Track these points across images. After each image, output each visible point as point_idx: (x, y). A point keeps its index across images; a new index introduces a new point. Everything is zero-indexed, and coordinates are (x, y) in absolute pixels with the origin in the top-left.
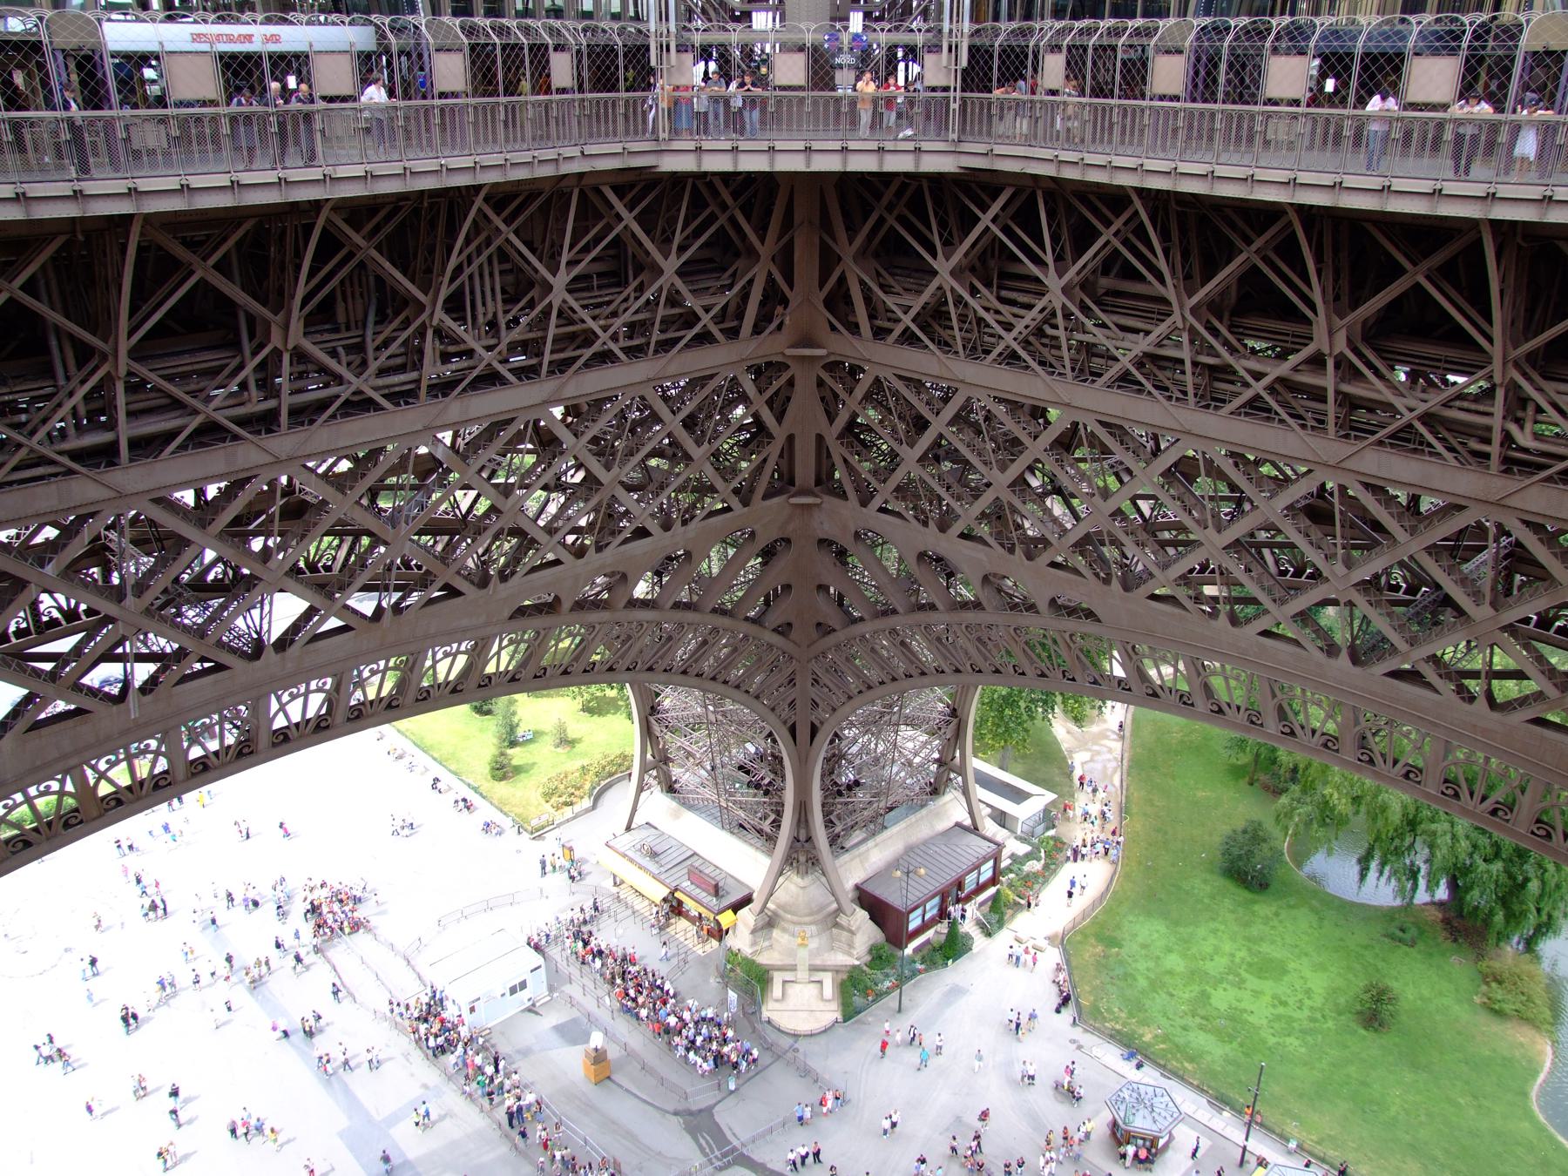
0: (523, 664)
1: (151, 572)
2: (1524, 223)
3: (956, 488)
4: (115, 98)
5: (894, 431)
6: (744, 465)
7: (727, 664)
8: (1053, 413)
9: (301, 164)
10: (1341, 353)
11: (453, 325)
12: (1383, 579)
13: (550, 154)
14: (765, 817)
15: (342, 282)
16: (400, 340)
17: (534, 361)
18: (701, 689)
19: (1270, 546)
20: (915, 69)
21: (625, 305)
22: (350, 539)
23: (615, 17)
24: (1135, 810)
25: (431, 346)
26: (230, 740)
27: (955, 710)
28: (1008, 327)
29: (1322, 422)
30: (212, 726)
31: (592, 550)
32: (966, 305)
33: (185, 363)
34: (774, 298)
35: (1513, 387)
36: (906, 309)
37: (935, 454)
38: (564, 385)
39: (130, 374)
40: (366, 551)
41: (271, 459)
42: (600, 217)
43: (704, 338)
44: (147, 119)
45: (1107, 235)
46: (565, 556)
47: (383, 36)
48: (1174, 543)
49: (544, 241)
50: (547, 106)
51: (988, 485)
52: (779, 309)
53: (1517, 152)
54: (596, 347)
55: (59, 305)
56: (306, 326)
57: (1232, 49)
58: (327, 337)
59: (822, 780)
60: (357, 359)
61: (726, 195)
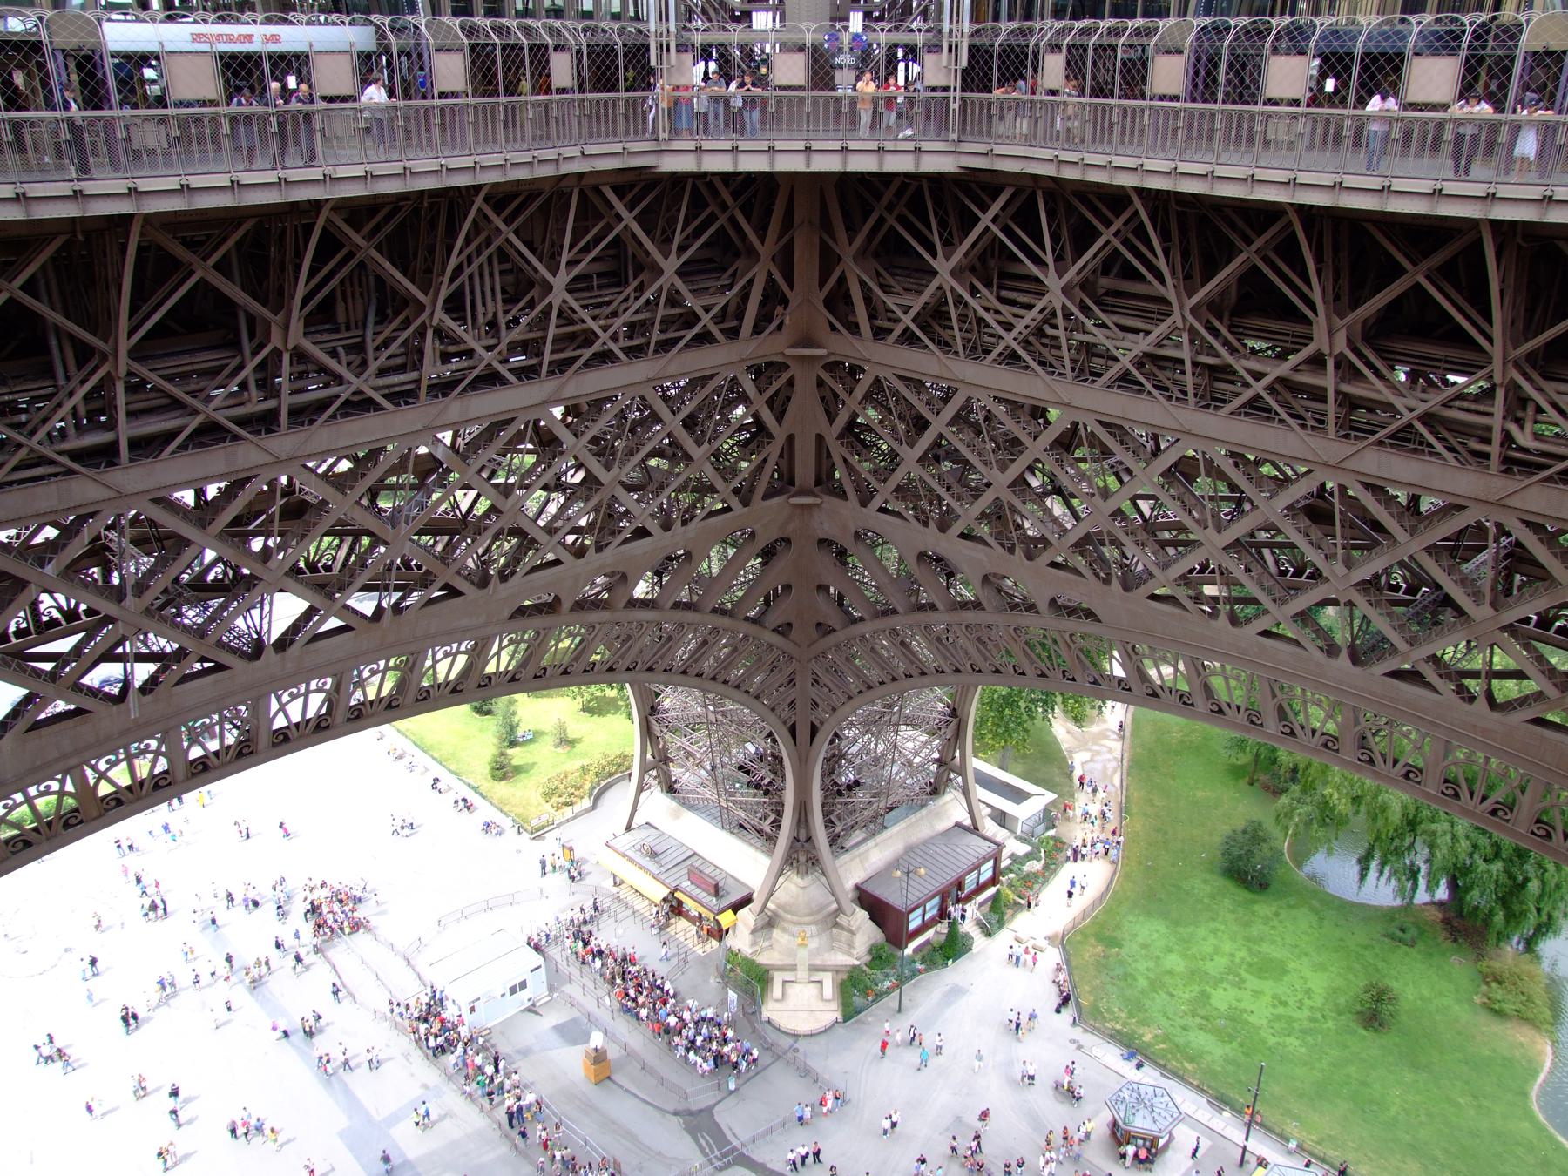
0: (523, 664)
1: (151, 572)
2: (1524, 223)
3: (956, 488)
4: (115, 98)
5: (894, 431)
6: (744, 465)
7: (727, 664)
8: (1053, 413)
9: (301, 164)
10: (1341, 353)
11: (453, 325)
12: (1383, 579)
13: (550, 154)
14: (765, 817)
15: (342, 282)
16: (400, 340)
17: (534, 361)
18: (701, 689)
19: (1270, 546)
20: (915, 69)
21: (625, 305)
22: (350, 539)
23: (615, 17)
24: (1135, 810)
25: (431, 346)
26: (230, 740)
27: (955, 710)
28: (1008, 327)
29: (1322, 422)
30: (212, 726)
31: (592, 550)
32: (966, 305)
33: (185, 363)
34: (774, 298)
35: (1513, 387)
36: (906, 309)
37: (935, 454)
38: (564, 385)
39: (130, 374)
40: (366, 551)
41: (271, 459)
42: (600, 217)
43: (704, 338)
44: (147, 119)
45: (1107, 235)
46: (565, 556)
47: (383, 36)
48: (1174, 543)
49: (544, 241)
50: (547, 106)
51: (988, 485)
52: (779, 309)
53: (1517, 152)
54: (596, 347)
55: (59, 305)
56: (306, 326)
57: (1232, 49)
58: (327, 337)
59: (822, 780)
60: (357, 359)
61: (726, 195)
